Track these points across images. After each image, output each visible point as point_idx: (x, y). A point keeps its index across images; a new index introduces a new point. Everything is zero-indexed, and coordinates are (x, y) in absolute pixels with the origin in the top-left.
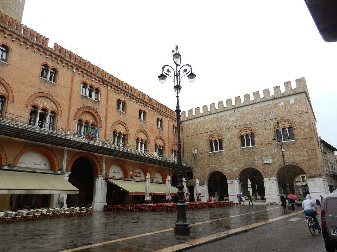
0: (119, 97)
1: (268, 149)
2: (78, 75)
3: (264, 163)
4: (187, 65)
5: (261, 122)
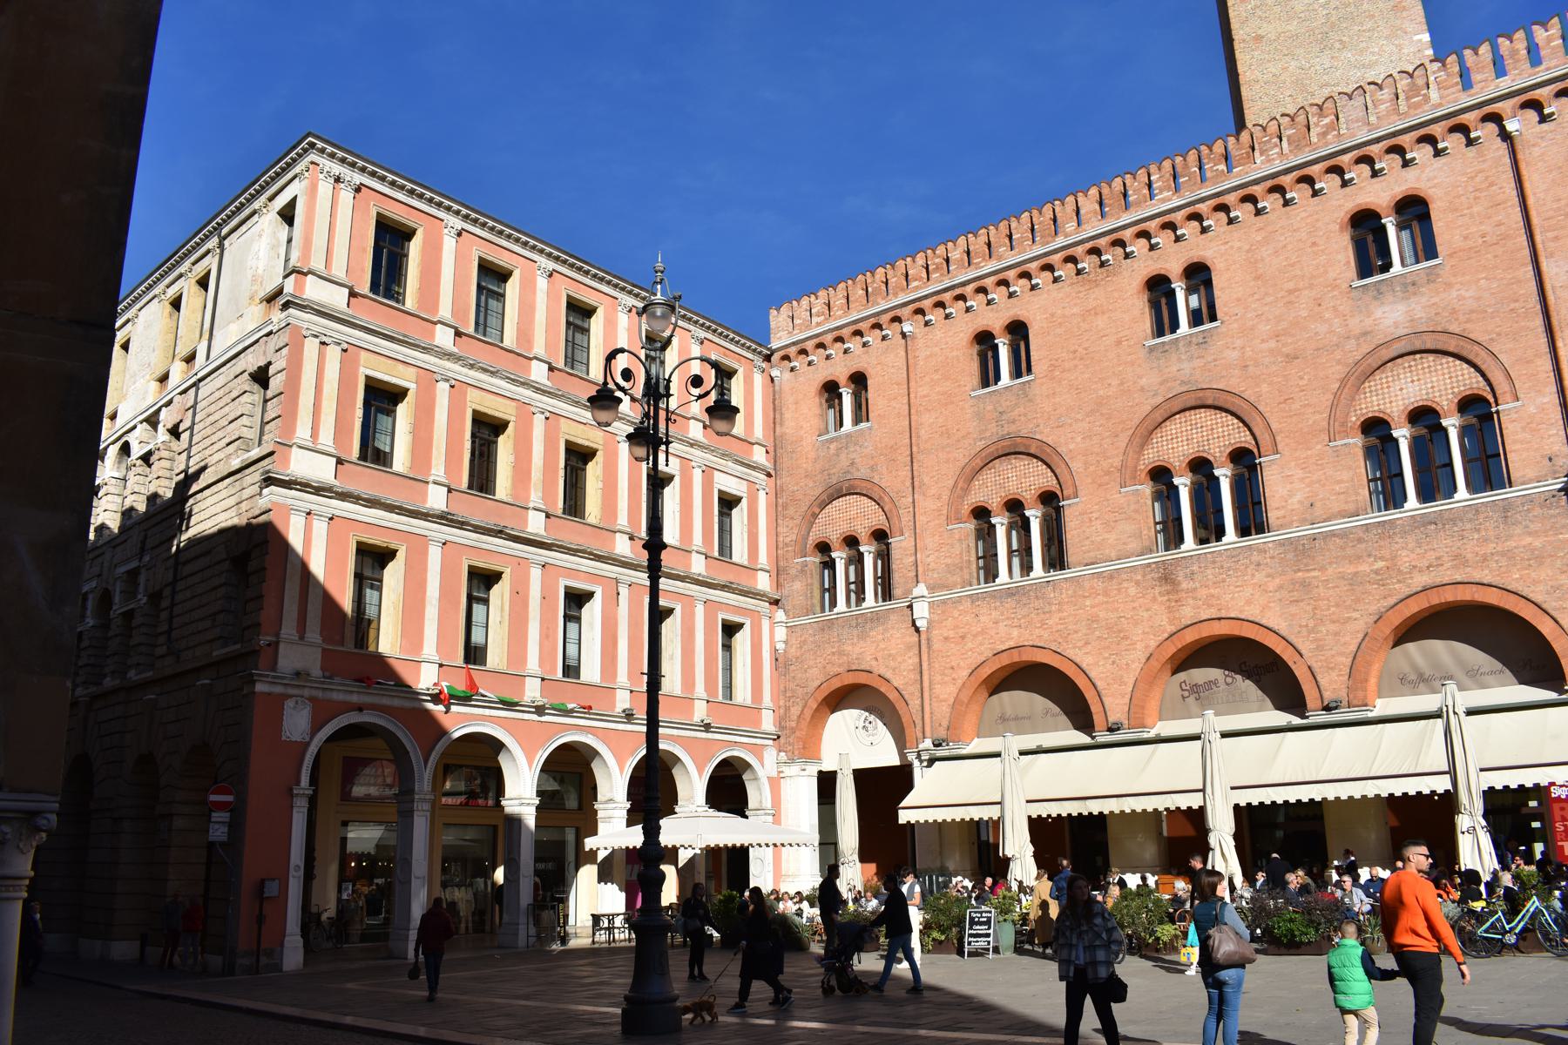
0: (1144, 264)
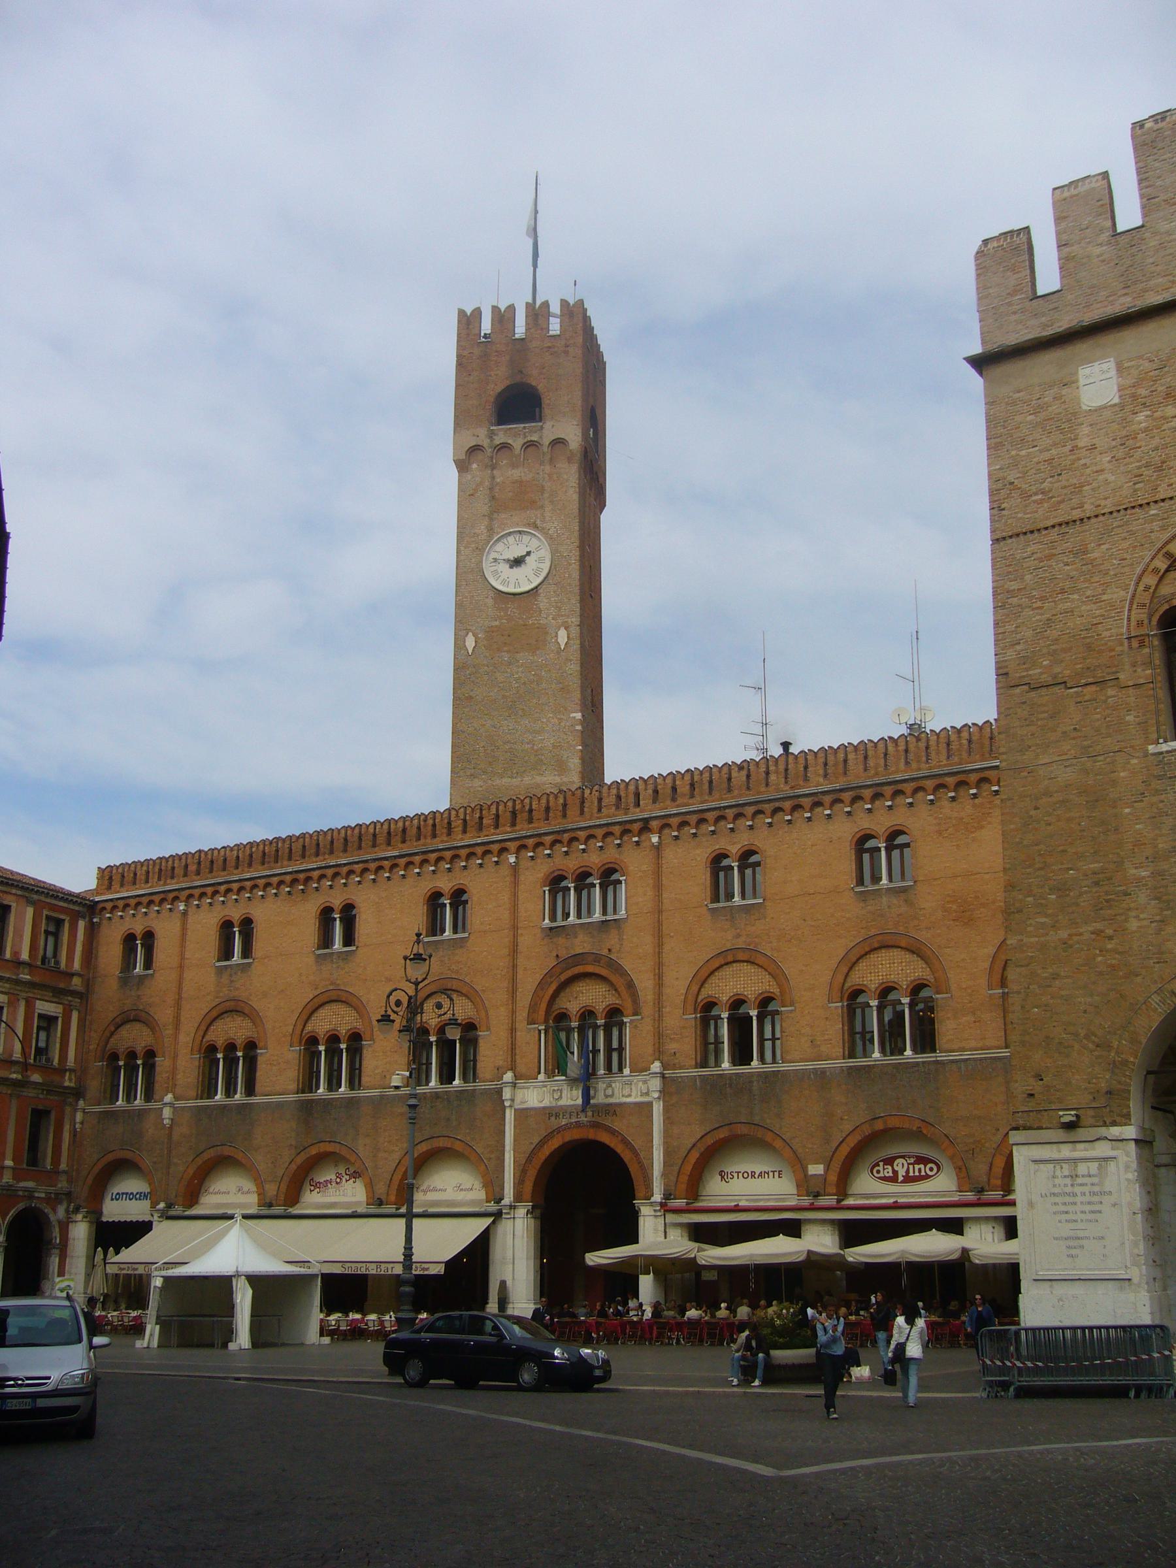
0: (427, 886)
2: (531, 863)
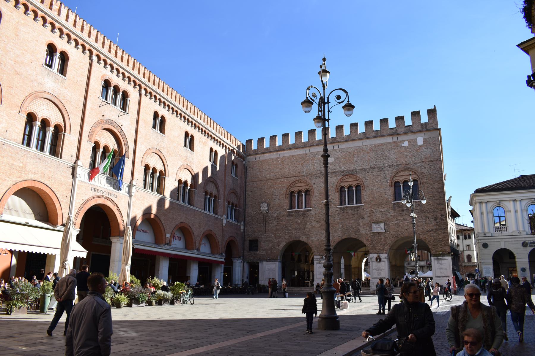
1: (381, 211)
3: (373, 232)
4: (340, 89)
5: (373, 168)
